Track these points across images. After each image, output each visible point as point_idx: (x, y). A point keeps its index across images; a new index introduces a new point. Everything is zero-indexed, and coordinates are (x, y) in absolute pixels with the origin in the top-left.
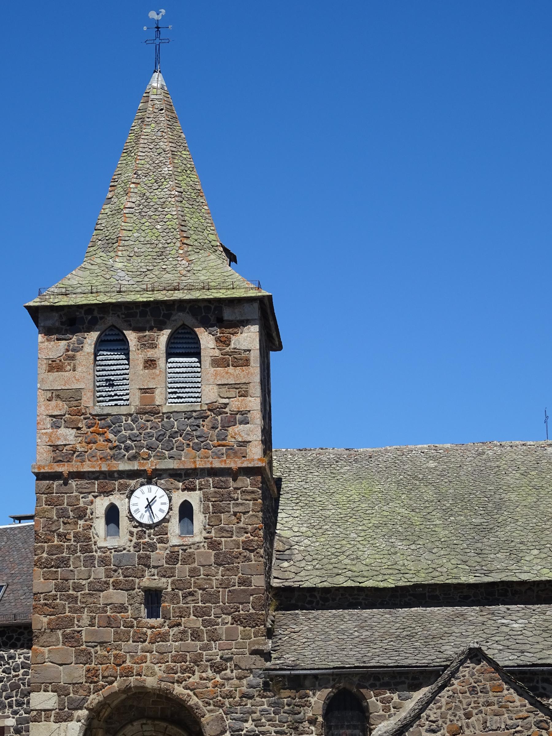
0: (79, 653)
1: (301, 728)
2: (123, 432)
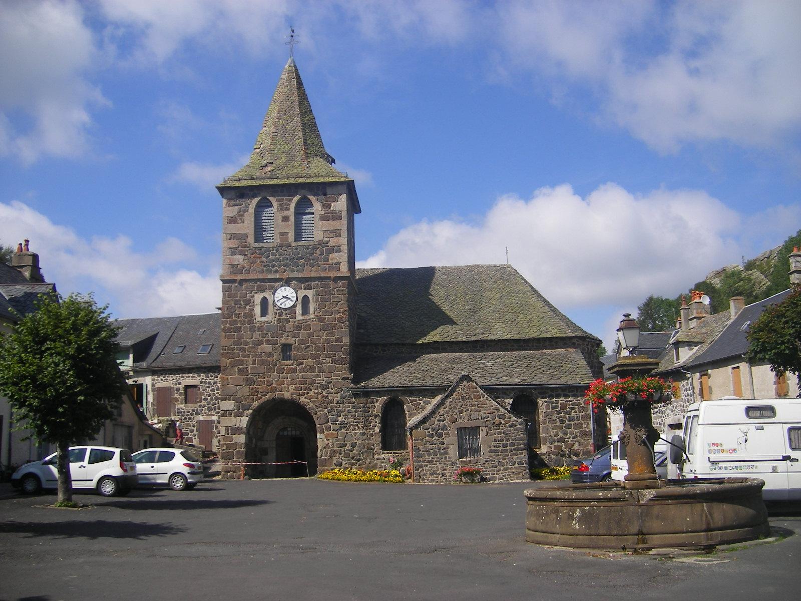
0: (247, 380)
2: (271, 257)
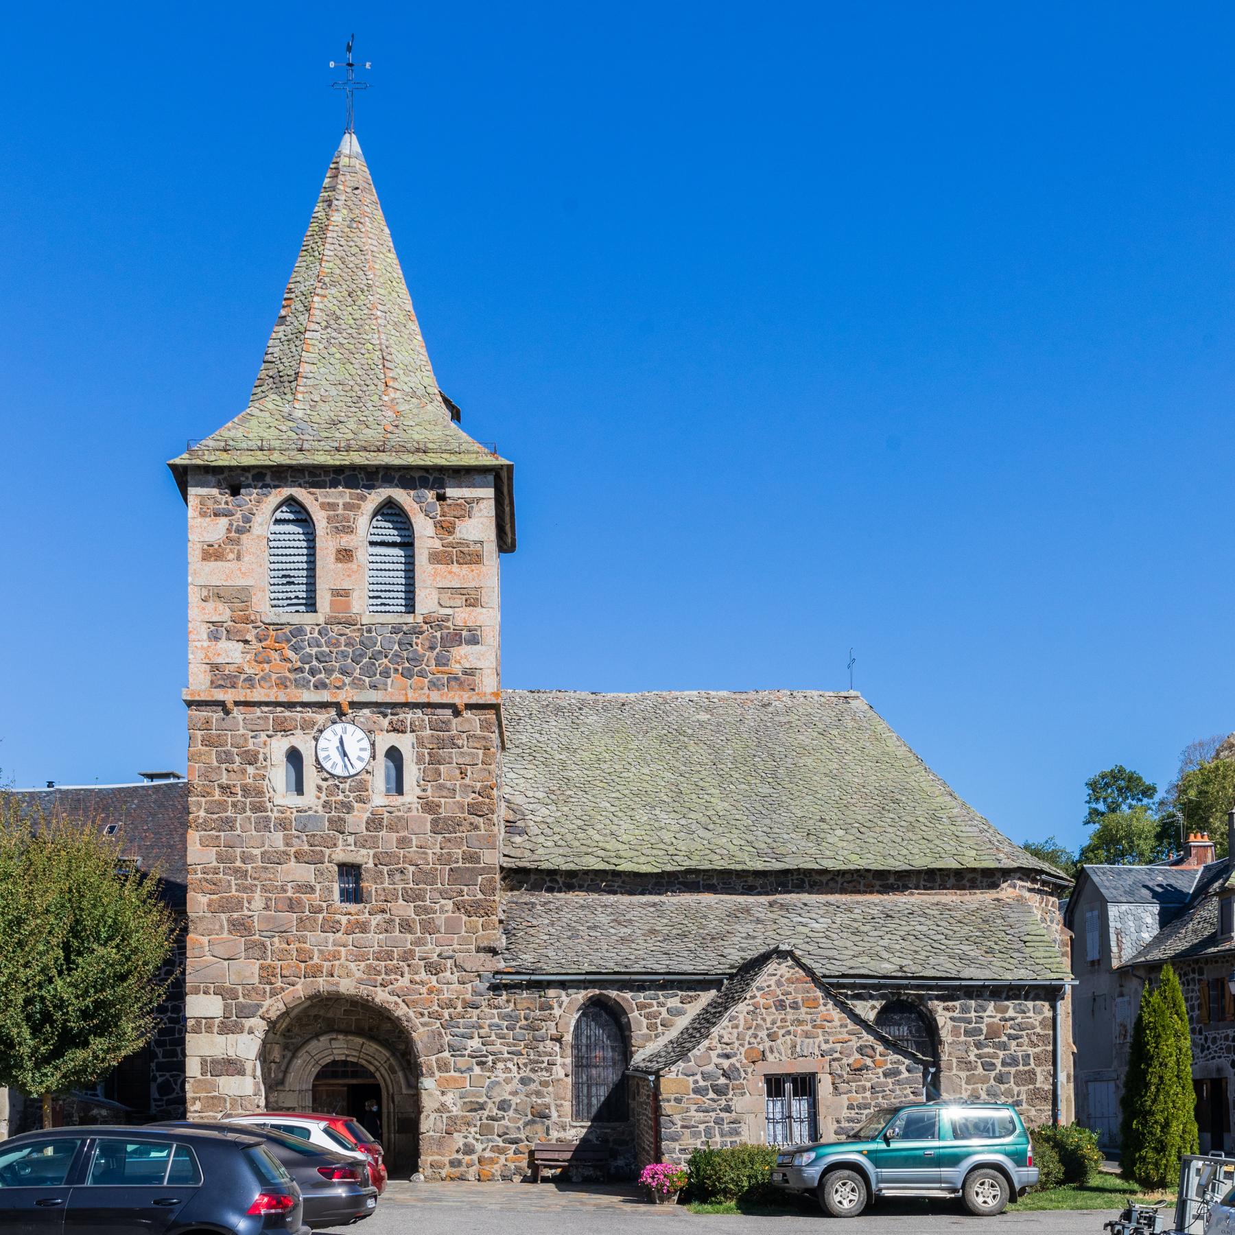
1: (541, 1048)
